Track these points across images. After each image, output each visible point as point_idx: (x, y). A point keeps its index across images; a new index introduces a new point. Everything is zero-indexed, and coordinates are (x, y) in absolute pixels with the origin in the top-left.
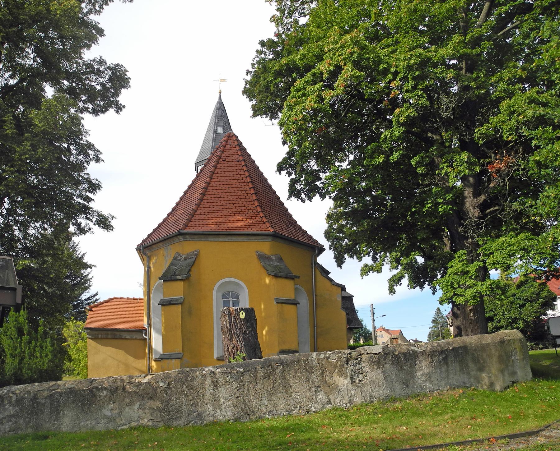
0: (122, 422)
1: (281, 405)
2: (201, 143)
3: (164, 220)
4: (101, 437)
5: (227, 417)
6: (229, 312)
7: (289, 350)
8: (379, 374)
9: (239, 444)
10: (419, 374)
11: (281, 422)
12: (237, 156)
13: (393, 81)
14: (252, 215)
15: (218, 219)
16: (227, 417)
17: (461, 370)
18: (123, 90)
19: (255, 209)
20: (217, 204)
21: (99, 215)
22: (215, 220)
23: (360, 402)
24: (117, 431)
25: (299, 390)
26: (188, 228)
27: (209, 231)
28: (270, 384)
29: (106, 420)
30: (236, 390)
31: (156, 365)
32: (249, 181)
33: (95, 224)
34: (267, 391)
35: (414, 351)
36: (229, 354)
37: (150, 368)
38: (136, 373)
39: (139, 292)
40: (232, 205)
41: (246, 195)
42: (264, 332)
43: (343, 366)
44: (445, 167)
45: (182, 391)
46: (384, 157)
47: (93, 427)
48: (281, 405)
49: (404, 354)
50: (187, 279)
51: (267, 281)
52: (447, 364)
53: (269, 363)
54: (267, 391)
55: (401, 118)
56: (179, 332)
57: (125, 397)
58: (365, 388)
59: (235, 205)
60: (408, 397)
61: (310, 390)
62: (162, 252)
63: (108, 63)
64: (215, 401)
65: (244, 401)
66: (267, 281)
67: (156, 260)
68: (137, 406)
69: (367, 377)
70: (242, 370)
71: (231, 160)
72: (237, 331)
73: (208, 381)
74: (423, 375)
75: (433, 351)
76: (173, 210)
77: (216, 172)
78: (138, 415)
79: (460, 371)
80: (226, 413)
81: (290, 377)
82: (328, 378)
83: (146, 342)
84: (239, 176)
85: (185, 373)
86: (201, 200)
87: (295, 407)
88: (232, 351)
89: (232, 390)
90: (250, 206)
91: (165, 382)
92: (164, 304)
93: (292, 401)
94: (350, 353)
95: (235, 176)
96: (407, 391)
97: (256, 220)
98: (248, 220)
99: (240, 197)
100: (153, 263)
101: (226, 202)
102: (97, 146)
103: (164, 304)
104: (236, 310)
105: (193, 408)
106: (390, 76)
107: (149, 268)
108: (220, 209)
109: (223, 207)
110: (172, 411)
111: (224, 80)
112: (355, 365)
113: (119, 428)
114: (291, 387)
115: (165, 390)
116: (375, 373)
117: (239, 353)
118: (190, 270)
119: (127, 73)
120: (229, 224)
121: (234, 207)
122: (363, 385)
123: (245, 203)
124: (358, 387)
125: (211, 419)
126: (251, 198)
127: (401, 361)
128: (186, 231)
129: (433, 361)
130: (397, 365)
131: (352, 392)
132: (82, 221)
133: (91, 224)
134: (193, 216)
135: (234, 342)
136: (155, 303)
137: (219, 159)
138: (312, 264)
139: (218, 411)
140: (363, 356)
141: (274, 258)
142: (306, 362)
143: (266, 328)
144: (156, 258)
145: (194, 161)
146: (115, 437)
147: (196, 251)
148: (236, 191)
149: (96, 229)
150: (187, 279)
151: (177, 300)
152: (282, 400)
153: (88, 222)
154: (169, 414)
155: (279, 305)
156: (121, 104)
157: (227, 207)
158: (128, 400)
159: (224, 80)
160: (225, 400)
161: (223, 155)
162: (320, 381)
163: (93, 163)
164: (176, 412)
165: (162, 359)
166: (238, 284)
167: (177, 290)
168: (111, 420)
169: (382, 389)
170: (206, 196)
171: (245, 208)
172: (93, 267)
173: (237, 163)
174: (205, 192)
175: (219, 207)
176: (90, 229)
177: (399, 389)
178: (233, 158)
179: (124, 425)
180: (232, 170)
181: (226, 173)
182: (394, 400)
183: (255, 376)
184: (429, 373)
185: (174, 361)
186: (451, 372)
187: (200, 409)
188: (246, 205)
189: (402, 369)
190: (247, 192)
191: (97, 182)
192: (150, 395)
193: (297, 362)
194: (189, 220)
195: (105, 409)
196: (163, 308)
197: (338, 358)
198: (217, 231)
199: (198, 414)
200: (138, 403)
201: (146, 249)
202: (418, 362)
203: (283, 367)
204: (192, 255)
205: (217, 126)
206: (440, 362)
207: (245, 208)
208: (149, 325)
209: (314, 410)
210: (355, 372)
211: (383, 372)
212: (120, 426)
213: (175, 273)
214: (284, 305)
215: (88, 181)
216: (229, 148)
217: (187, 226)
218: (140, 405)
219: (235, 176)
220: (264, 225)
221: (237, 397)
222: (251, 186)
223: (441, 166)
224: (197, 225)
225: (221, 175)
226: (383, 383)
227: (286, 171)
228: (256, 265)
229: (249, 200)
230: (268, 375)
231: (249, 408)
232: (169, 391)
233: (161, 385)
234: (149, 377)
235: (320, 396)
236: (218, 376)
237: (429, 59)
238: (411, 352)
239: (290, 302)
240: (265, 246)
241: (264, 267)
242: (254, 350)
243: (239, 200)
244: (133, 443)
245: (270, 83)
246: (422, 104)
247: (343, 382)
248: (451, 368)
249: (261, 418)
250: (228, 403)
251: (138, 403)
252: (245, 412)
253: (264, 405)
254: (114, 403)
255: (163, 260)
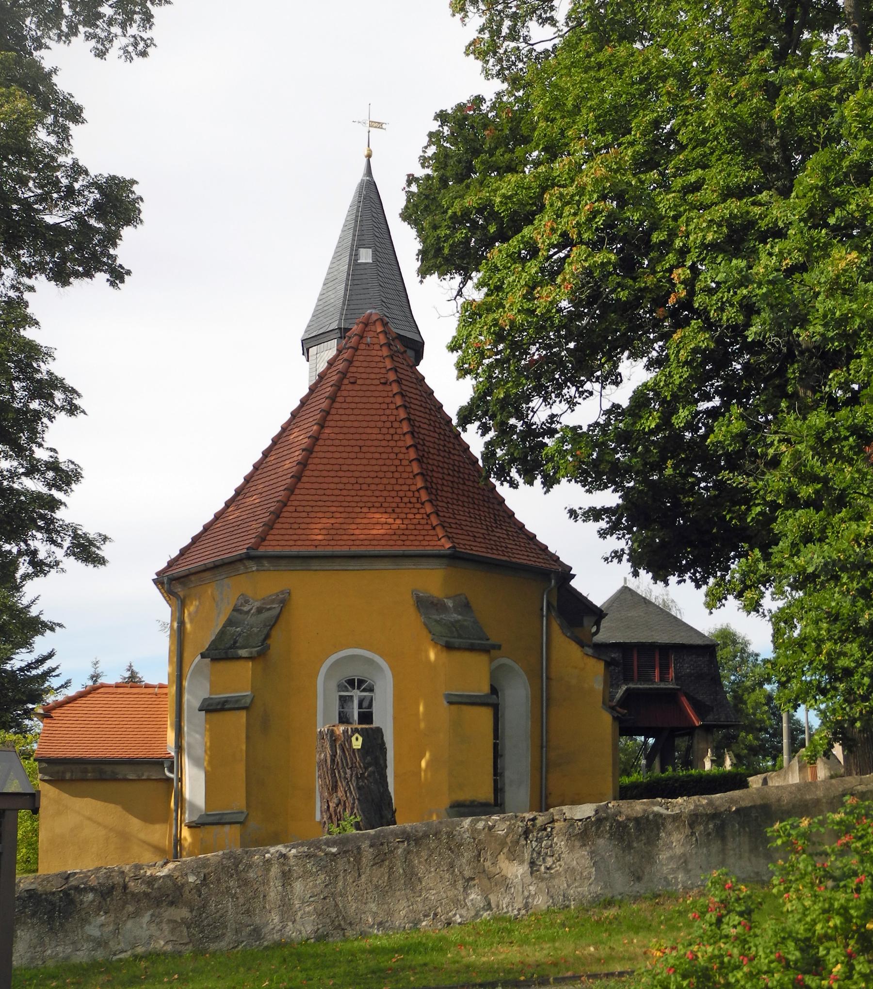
0: (119, 947)
1: (402, 912)
2: (316, 296)
3: (218, 516)
4: (84, 972)
5: (304, 934)
6: (331, 736)
7: (472, 802)
8: (583, 856)
9: (311, 973)
10: (663, 856)
11: (398, 939)
12: (384, 371)
13: (677, 267)
14: (407, 510)
15: (333, 521)
16: (304, 934)
17: (754, 850)
18: (127, 232)
19: (417, 494)
20: (332, 486)
21: (76, 536)
22: (327, 522)
23: (544, 907)
24: (111, 963)
25: (435, 887)
26: (266, 543)
27: (312, 550)
28: (383, 875)
29: (91, 945)
30: (323, 885)
31: (193, 835)
32: (405, 430)
33: (67, 555)
34: (377, 887)
35: (658, 815)
36: (330, 817)
37: (178, 841)
38: (147, 857)
39: (157, 671)
40: (365, 487)
41: (397, 462)
42: (423, 764)
43: (518, 842)
44: (776, 443)
45: (228, 888)
46: (659, 418)
47: (67, 958)
48: (402, 911)
49: (637, 820)
50: (261, 655)
51: (432, 656)
52: (723, 839)
53: (384, 837)
54: (377, 887)
55: (682, 352)
56: (241, 769)
57: (126, 903)
58: (556, 882)
59: (373, 487)
60: (637, 898)
61: (454, 884)
62: (209, 590)
63: (93, 172)
64: (285, 907)
65: (336, 905)
66: (432, 656)
67: (198, 607)
68: (146, 918)
69: (562, 863)
70: (334, 850)
71: (368, 382)
72: (345, 773)
73: (275, 870)
74: (671, 858)
75: (696, 815)
76: (239, 492)
77: (333, 411)
78: (149, 933)
79: (751, 851)
80: (303, 926)
81: (420, 862)
82: (488, 864)
83: (171, 787)
84: (384, 418)
85: (235, 858)
86: (298, 477)
87: (425, 916)
88: (335, 811)
89: (315, 886)
90: (405, 488)
91: (197, 875)
92: (211, 708)
93: (420, 905)
94: (534, 819)
95: (377, 418)
96: (638, 887)
97: (416, 521)
98: (399, 521)
99: (385, 468)
100: (190, 614)
101: (353, 480)
102: (69, 382)
103: (211, 708)
104: (345, 732)
105: (245, 919)
106: (671, 258)
107: (182, 623)
108: (339, 498)
109: (345, 492)
110: (209, 925)
111: (379, 125)
112: (539, 840)
113: (115, 958)
114: (420, 880)
115: (198, 889)
116: (577, 855)
117: (348, 812)
118: (268, 636)
119: (135, 188)
120: (357, 532)
121: (369, 493)
122: (552, 877)
123: (393, 481)
124: (542, 879)
125: (276, 937)
126: (408, 469)
127: (629, 834)
128: (262, 550)
129: (693, 834)
130: (621, 839)
131: (531, 888)
132: (39, 543)
133: (59, 553)
134: (277, 515)
135: (340, 794)
136: (192, 700)
137: (341, 381)
138: (542, 609)
139: (290, 924)
140: (556, 824)
141: (450, 604)
142: (450, 835)
143: (428, 755)
144: (196, 602)
145: (299, 333)
146: (107, 971)
147: (282, 592)
148: (377, 456)
149: (71, 564)
150: (261, 655)
151: (238, 700)
152: (404, 903)
153: (53, 548)
154: (203, 930)
155: (454, 707)
156: (120, 266)
157: (353, 493)
158: (131, 908)
159: (379, 125)
160: (303, 903)
161: (352, 369)
162: (474, 868)
163: (61, 417)
164: (215, 927)
165: (204, 824)
166: (370, 662)
167: (240, 678)
168: (101, 943)
169: (587, 883)
170: (310, 467)
171: (393, 494)
172: (57, 628)
173: (381, 388)
174: (309, 458)
175: (337, 492)
176: (57, 563)
177: (621, 883)
178: (373, 376)
179: (122, 952)
180: (368, 406)
181: (356, 412)
182: (609, 903)
183: (358, 861)
184: (684, 855)
185: (227, 828)
186: (731, 852)
187: (257, 920)
188: (397, 488)
189: (630, 847)
190: (401, 456)
191: (72, 466)
192: (171, 898)
193: (435, 835)
194: (270, 526)
195: (90, 924)
196: (210, 716)
197: (509, 828)
198: (329, 550)
199: (254, 930)
200: (150, 913)
201: (174, 581)
202: (663, 835)
203: (409, 845)
204: (273, 602)
205: (359, 246)
206: (709, 834)
207: (393, 494)
208: (179, 748)
209: (459, 920)
210: (539, 853)
211: (592, 852)
212: (115, 954)
213: (235, 642)
214: (464, 707)
215: (54, 466)
216: (365, 353)
217: (264, 540)
218: (152, 915)
219: (377, 418)
220: (432, 532)
221: (324, 898)
222: (409, 442)
223: (769, 441)
224: (287, 537)
225: (345, 418)
226: (590, 873)
227: (477, 424)
228: (412, 621)
229: (405, 475)
230: (380, 860)
231: (344, 918)
232: (204, 890)
233: (191, 879)
234: (171, 866)
235: (472, 896)
236: (292, 861)
237: (752, 223)
238: (651, 817)
239: (478, 700)
240: (433, 580)
241: (425, 624)
242: (377, 808)
243: (381, 475)
244: (139, 978)
245: (444, 242)
246: (728, 320)
247: (516, 871)
248: (730, 845)
249: (364, 935)
250: (307, 909)
251: (150, 913)
252: (336, 923)
253: (370, 912)
254: (106, 913)
255: (212, 612)
